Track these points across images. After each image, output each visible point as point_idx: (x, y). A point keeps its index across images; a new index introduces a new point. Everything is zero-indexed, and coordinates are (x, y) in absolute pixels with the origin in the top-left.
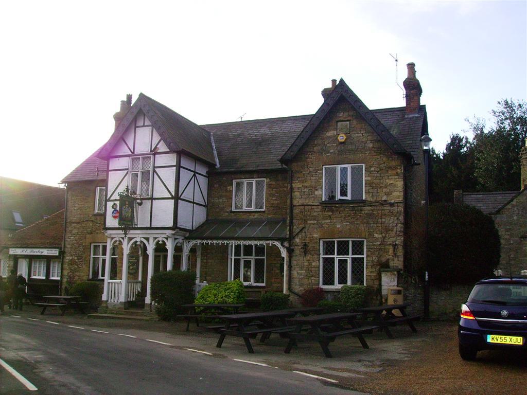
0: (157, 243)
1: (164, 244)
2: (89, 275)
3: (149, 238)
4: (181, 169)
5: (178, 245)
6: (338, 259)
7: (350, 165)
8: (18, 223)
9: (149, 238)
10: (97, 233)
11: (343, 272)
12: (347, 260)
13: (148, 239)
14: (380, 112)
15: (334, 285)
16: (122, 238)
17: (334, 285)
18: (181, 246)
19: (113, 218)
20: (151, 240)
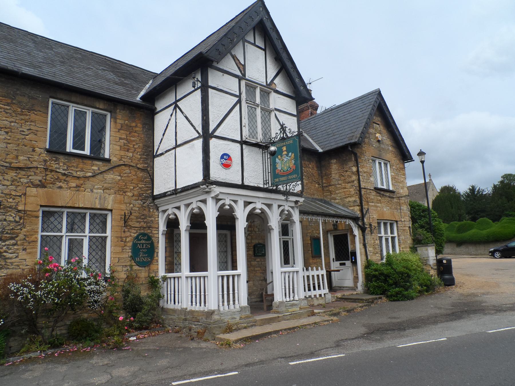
0: (221, 209)
1: (232, 209)
2: (397, 227)
3: (272, 205)
4: (178, 143)
5: (170, 217)
6: (74, 108)
7: (91, 109)
8: (121, 115)
9: (272, 205)
10: (60, 187)
11: (221, 48)
12: (86, 112)
13: (269, 206)
14: (463, 254)
15: (288, 235)
16: (176, 208)
17: (288, 235)
18: (321, 170)
19: (220, 167)
20: (275, 207)
